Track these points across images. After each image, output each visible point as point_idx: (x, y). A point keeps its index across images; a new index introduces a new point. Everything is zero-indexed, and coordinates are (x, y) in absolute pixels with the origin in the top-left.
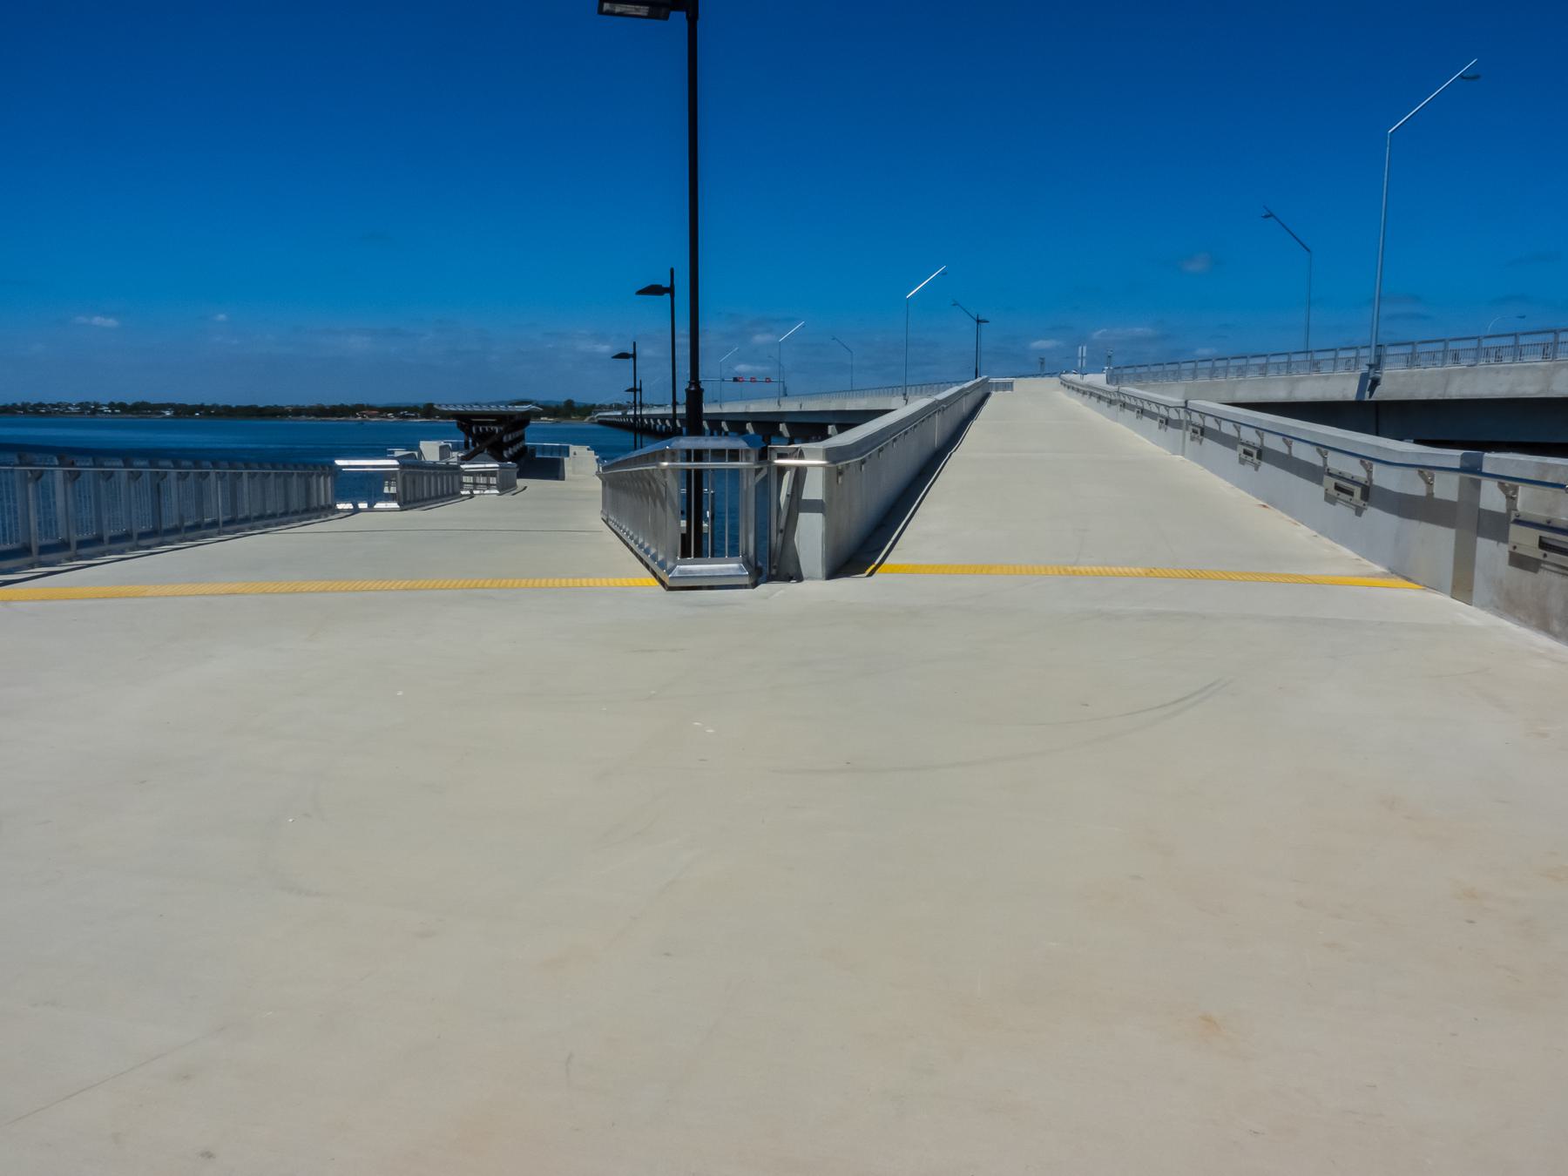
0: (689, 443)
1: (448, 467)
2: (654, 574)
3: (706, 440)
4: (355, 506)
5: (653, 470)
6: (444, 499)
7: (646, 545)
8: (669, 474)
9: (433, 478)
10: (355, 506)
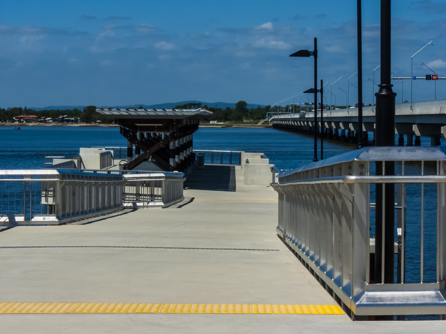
0: (379, 154)
1: (109, 177)
2: (339, 301)
3: (399, 151)
4: (12, 219)
5: (339, 183)
6: (104, 212)
7: (329, 267)
8: (357, 188)
9: (93, 189)
10: (12, 219)
